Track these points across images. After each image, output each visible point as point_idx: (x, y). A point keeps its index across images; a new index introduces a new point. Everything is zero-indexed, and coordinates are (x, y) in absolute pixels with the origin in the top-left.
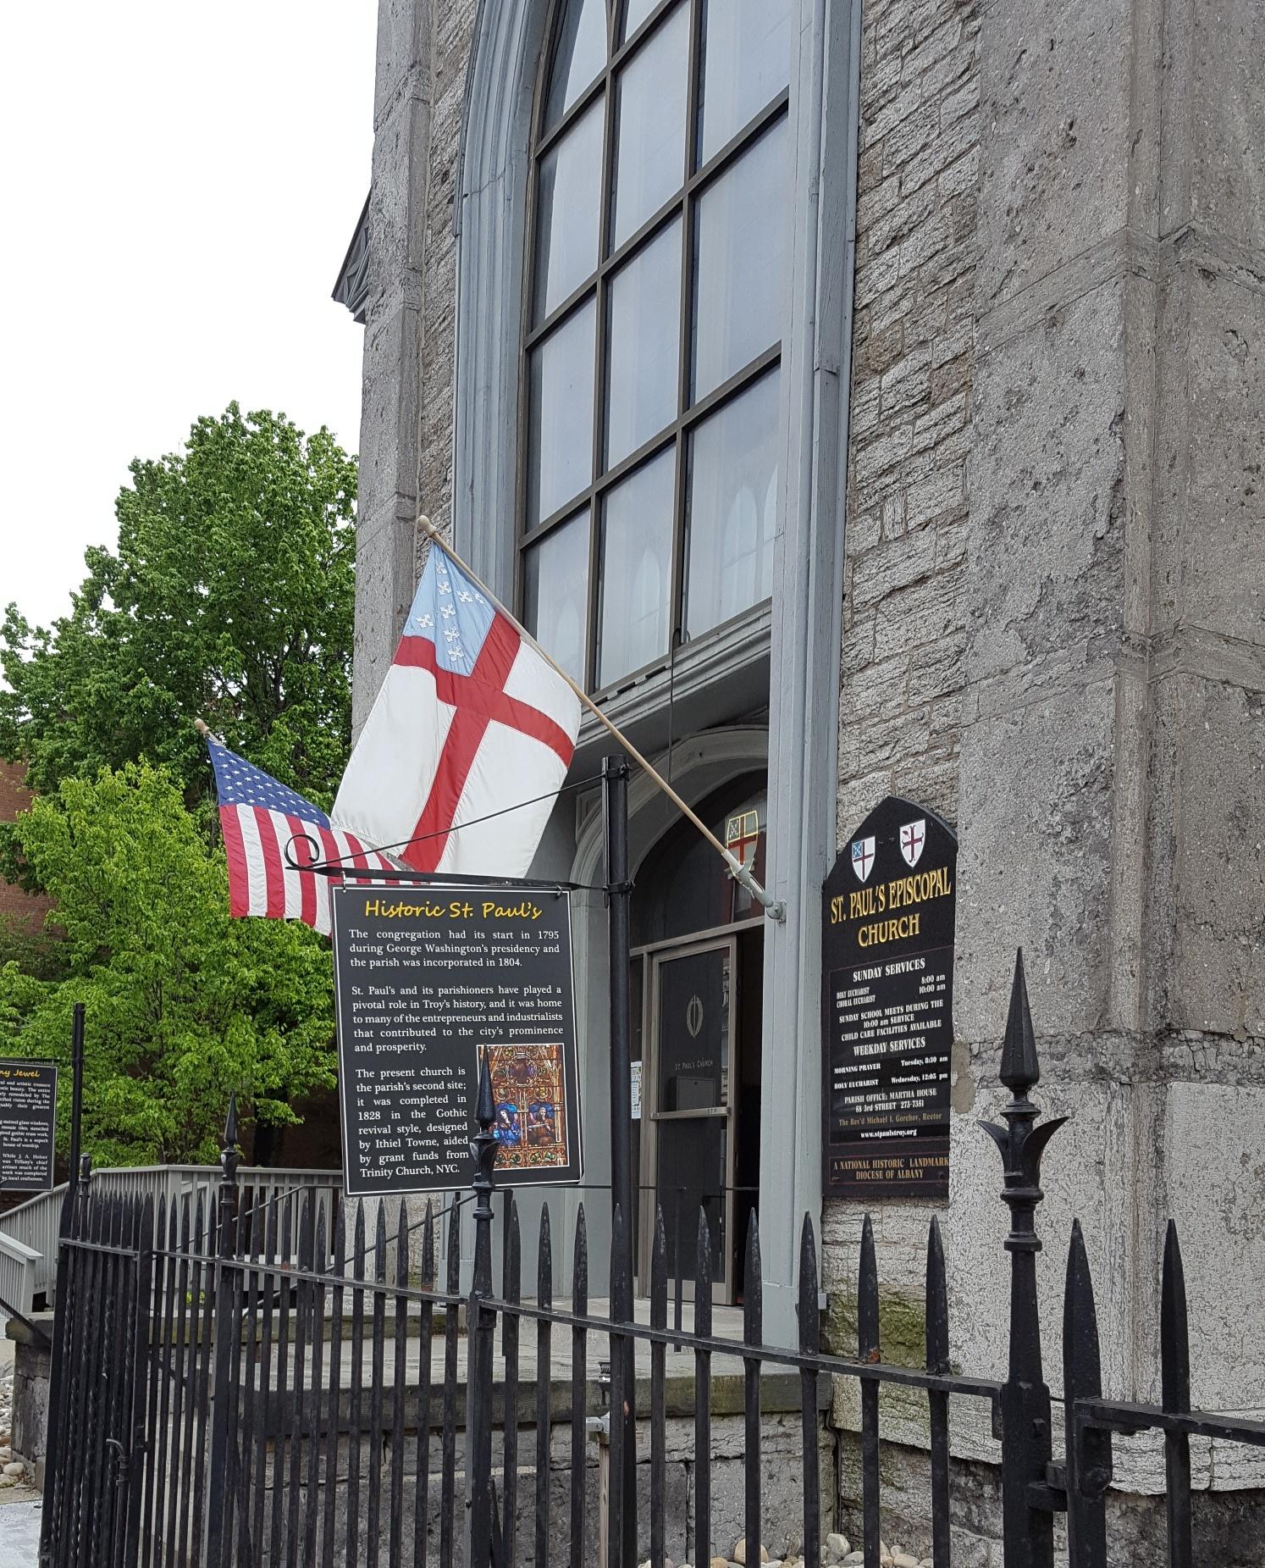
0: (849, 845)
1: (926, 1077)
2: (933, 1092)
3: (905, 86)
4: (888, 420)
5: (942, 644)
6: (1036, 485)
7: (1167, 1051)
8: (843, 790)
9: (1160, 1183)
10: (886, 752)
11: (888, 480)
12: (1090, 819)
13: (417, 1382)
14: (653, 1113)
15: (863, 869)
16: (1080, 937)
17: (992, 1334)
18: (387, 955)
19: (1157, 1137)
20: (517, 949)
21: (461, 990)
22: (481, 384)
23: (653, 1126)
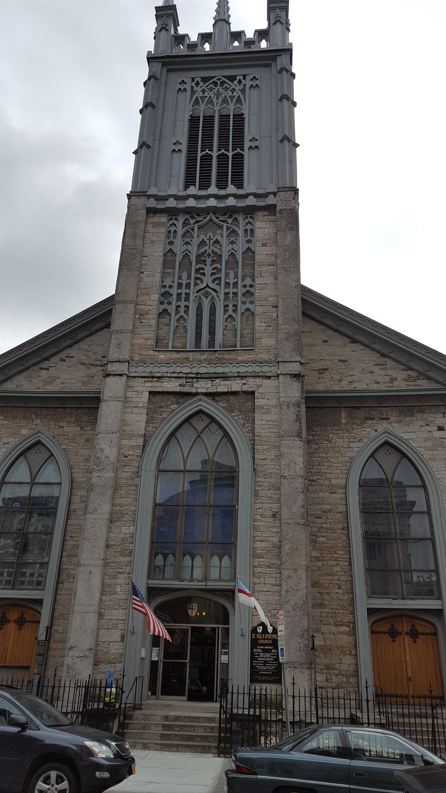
0: (256, 626)
4: (259, 566)
11: (261, 574)
14: (162, 659)
23: (162, 663)
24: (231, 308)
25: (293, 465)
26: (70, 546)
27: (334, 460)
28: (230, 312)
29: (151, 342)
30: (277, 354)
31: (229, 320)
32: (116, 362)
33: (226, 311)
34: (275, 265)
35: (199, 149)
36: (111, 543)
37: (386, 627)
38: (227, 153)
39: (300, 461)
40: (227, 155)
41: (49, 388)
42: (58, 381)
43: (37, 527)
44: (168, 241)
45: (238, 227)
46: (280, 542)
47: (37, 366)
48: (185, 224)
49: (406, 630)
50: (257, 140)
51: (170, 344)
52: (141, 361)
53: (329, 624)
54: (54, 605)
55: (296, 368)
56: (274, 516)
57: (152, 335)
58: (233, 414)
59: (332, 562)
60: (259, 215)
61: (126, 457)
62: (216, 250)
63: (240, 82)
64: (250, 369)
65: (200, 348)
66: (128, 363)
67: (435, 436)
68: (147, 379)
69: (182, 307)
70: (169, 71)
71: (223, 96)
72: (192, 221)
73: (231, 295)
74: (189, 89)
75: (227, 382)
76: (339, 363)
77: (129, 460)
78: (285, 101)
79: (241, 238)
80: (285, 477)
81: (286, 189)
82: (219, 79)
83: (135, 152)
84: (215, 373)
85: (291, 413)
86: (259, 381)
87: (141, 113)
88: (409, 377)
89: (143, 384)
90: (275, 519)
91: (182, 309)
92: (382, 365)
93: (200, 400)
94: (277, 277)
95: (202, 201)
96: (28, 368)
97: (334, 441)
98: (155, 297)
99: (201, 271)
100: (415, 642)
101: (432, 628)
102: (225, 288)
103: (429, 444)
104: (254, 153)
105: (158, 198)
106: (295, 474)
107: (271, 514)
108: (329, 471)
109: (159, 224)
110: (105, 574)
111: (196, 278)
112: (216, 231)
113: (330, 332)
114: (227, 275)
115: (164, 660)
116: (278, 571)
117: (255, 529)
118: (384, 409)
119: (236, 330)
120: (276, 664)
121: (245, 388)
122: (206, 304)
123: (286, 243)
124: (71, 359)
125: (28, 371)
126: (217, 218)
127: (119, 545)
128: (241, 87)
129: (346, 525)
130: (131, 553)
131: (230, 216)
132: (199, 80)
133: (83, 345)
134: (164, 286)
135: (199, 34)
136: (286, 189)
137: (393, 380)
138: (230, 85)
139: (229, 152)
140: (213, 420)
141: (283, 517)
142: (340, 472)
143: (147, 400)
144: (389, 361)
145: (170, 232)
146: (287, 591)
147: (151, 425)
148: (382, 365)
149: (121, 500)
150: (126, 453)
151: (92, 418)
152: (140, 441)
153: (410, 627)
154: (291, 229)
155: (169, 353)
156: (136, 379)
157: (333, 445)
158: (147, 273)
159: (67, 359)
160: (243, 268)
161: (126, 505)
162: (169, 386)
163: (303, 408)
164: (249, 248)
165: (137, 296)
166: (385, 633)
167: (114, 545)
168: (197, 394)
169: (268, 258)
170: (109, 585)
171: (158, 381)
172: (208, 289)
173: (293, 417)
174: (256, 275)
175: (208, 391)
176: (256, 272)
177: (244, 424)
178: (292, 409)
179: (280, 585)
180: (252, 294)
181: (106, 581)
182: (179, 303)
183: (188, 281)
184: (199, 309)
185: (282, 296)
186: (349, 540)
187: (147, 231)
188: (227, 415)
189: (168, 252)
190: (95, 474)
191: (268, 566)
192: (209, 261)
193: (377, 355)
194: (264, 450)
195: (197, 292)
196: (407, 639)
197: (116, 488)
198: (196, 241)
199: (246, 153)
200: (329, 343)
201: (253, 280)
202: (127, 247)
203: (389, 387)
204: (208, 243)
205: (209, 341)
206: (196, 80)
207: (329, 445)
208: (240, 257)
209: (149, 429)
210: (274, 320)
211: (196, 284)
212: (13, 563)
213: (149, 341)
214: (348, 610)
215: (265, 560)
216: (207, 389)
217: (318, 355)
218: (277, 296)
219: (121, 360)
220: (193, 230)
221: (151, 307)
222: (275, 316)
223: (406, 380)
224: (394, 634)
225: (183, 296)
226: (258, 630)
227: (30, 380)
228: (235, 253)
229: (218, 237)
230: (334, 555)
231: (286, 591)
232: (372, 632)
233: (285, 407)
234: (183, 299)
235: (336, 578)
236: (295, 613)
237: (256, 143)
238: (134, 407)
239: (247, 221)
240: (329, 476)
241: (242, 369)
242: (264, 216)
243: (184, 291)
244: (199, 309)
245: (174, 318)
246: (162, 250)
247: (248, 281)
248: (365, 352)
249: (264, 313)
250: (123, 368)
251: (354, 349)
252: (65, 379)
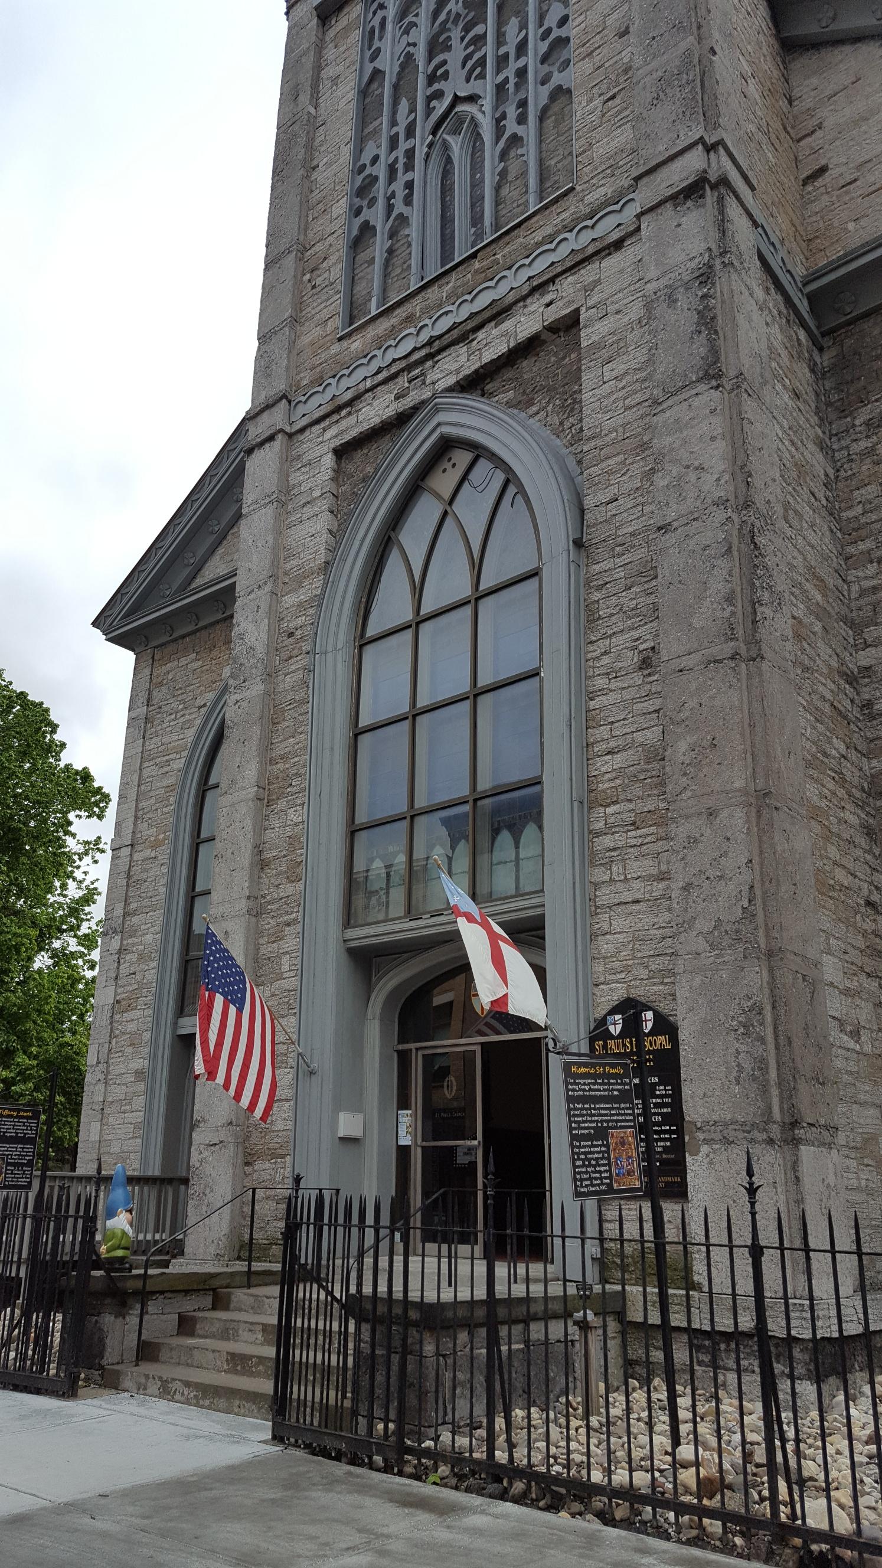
0: (605, 1016)
1: (663, 1136)
2: (668, 1144)
3: (612, 691)
4: (609, 829)
5: (652, 932)
6: (707, 878)
7: (797, 1132)
8: (596, 989)
9: (799, 1192)
10: (623, 975)
11: (613, 854)
12: (753, 1026)
13: (485, 1297)
15: (615, 1029)
16: (754, 1079)
17: (720, 1266)
18: (580, 1090)
19: (795, 1171)
20: (617, 1087)
21: (602, 1106)
22: (327, 745)
23: (419, 1150)
25: (692, 477)
36: (268, 855)
66: (284, 401)
89: (321, 439)
90: (646, 672)
106: (698, 504)
107: (635, 660)
110: (259, 933)
115: (425, 1144)
120: (670, 1132)
121: (554, 314)
127: (285, 856)
146: (687, 888)
167: (276, 858)
170: (269, 959)
171: (349, 414)
177: (561, 423)
188: (501, 415)
191: (634, 824)
194: (610, 473)
216: (458, 371)
219: (271, 401)
226: (611, 1028)
227: (230, 558)
231: (684, 888)
236: (717, 956)
249: (599, 68)
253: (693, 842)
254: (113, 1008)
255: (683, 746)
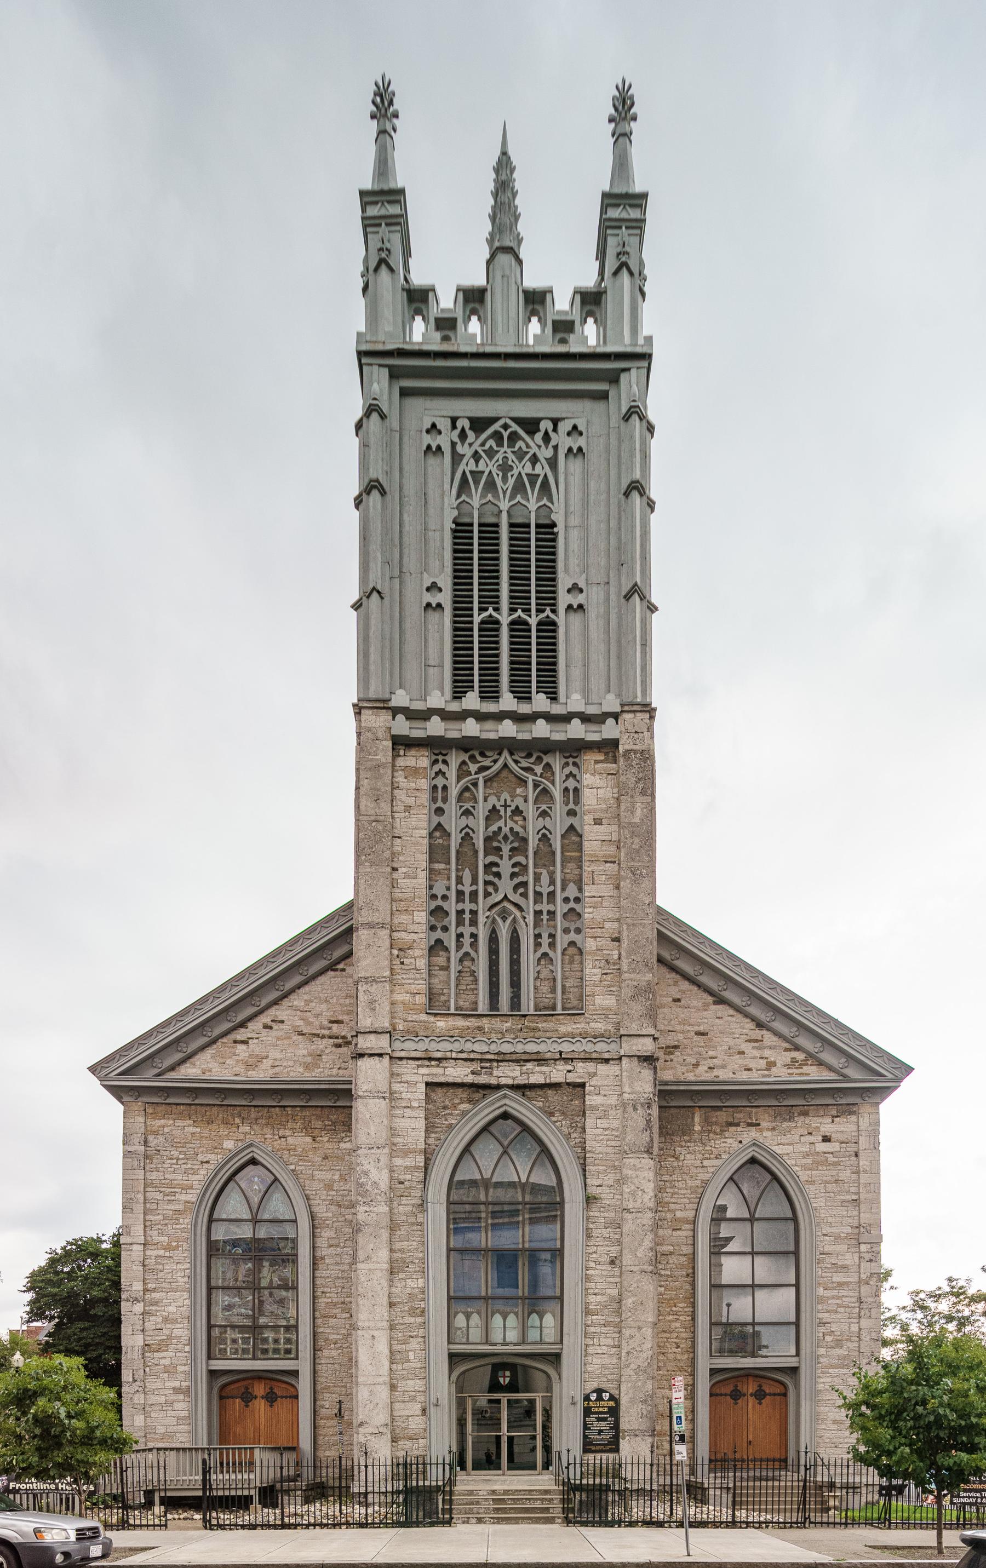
4: (593, 1325)
24: (545, 940)
25: (640, 1193)
26: (323, 1305)
27: (680, 1185)
28: (545, 948)
29: (421, 999)
30: (619, 1023)
31: (543, 962)
32: (370, 1032)
33: (538, 945)
34: (614, 862)
35: (476, 606)
37: (728, 1389)
38: (528, 618)
39: (650, 1188)
40: (526, 623)
41: (254, 1075)
42: (267, 1063)
43: (271, 1280)
44: (434, 807)
45: (553, 783)
46: (620, 1294)
47: (228, 1036)
48: (462, 772)
49: (750, 1391)
50: (581, 591)
51: (452, 1002)
52: (408, 1032)
53: (663, 1388)
54: (314, 1377)
55: (646, 1047)
56: (612, 1262)
57: (423, 987)
58: (554, 1119)
59: (671, 1317)
60: (589, 758)
61: (401, 1183)
62: (517, 828)
63: (547, 438)
64: (578, 1047)
65: (498, 1010)
67: (817, 1150)
68: (420, 1063)
69: (467, 936)
70: (404, 393)
71: (515, 472)
72: (473, 768)
73: (545, 917)
74: (447, 449)
75: (544, 1069)
76: (696, 1038)
77: (407, 1188)
78: (635, 495)
79: (559, 808)
80: (628, 1211)
81: (635, 708)
82: (506, 427)
83: (357, 606)
84: (525, 1053)
85: (638, 1118)
86: (591, 1067)
87: (357, 507)
88: (794, 1060)
91: (467, 940)
92: (756, 1041)
93: (505, 1096)
94: (619, 884)
95: (489, 725)
96: (214, 1042)
97: (682, 1158)
98: (422, 917)
99: (495, 869)
100: (760, 1403)
101: (782, 1387)
102: (535, 902)
103: (809, 1161)
104: (576, 618)
105: (411, 715)
108: (673, 1200)
109: (413, 772)
110: (391, 1339)
111: (487, 883)
112: (515, 789)
113: (685, 985)
114: (537, 878)
116: (616, 1330)
117: (588, 1279)
118: (754, 1110)
119: (554, 980)
121: (572, 1078)
122: (504, 932)
123: (634, 821)
124: (280, 1025)
125: (215, 1046)
126: (516, 762)
128: (549, 453)
129: (691, 1271)
130: (423, 1312)
131: (539, 759)
132: (467, 424)
133: (297, 1000)
134: (434, 897)
135: (458, 290)
136: (635, 708)
137: (771, 1065)
138: (528, 446)
139: (530, 616)
140: (526, 1128)
141: (624, 1263)
142: (688, 1201)
143: (423, 1097)
144: (767, 1035)
145: (435, 787)
146: (628, 1353)
147: (433, 1135)
148: (756, 1041)
149: (400, 1244)
150: (402, 1177)
151: (327, 1123)
152: (420, 1161)
153: (756, 1388)
154: (643, 793)
155: (451, 1019)
156: (404, 1062)
157: (681, 1164)
158: (404, 870)
159: (275, 1026)
160: (563, 866)
161: (409, 1251)
162: (455, 1074)
163: (655, 1111)
164: (572, 827)
165: (392, 914)
166: (726, 1395)
167: (399, 1303)
168: (498, 1087)
169: (604, 848)
171: (438, 1066)
172: (506, 904)
173: (642, 1123)
174: (585, 880)
175: (516, 1082)
176: (585, 875)
178: (640, 1111)
179: (619, 1346)
180: (579, 915)
181: (394, 1347)
182: (460, 929)
183: (474, 888)
184: (493, 939)
185: (629, 921)
186: (694, 1289)
187: (396, 785)
189: (435, 829)
190: (362, 1209)
192: (506, 849)
193: (752, 1025)
195: (489, 910)
196: (751, 1400)
197: (393, 1227)
198: (482, 810)
199: (561, 619)
200: (683, 1002)
201: (580, 890)
202: (365, 818)
203: (764, 1076)
204: (502, 813)
205: (512, 999)
206: (459, 424)
207: (675, 1164)
208: (557, 845)
209: (431, 1141)
210: (614, 964)
211: (487, 894)
212: (248, 1326)
213: (417, 997)
214: (686, 1371)
215: (599, 1317)
216: (514, 1078)
217: (666, 1023)
218: (618, 920)
219: (379, 1030)
220: (475, 785)
221: (415, 936)
222: (616, 957)
223: (788, 1066)
224: (736, 1395)
225: (467, 916)
226: (501, 1380)
227: (222, 1061)
228: (549, 836)
229: (519, 801)
230: (674, 1309)
232: (711, 1395)
233: (630, 1109)
234: (467, 922)
235: (675, 1335)
237: (581, 599)
238: (405, 1107)
239: (567, 771)
240: (672, 1206)
241: (566, 1047)
242: (597, 762)
243: (468, 906)
244: (493, 939)
245: (454, 956)
246: (425, 824)
247: (572, 891)
248: (734, 1019)
250: (381, 1043)
251: (719, 1015)
252: (275, 1060)
253: (631, 1337)
254: (143, 1349)
255: (630, 1301)
